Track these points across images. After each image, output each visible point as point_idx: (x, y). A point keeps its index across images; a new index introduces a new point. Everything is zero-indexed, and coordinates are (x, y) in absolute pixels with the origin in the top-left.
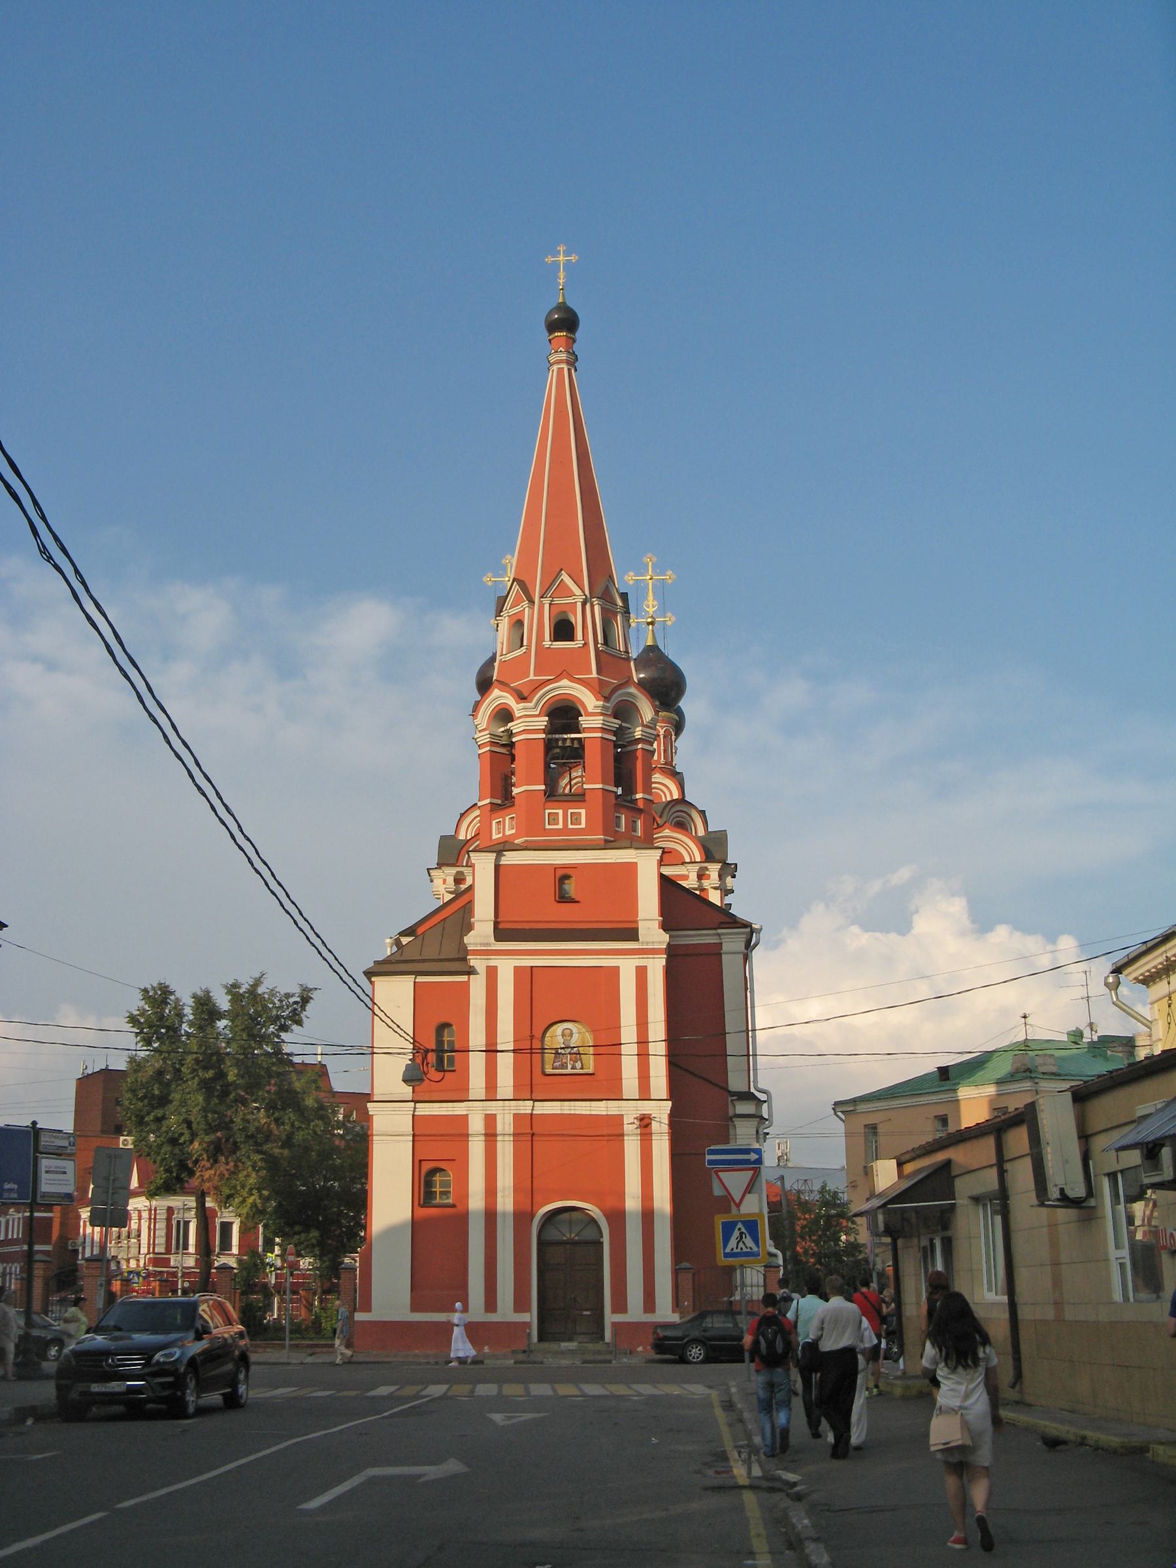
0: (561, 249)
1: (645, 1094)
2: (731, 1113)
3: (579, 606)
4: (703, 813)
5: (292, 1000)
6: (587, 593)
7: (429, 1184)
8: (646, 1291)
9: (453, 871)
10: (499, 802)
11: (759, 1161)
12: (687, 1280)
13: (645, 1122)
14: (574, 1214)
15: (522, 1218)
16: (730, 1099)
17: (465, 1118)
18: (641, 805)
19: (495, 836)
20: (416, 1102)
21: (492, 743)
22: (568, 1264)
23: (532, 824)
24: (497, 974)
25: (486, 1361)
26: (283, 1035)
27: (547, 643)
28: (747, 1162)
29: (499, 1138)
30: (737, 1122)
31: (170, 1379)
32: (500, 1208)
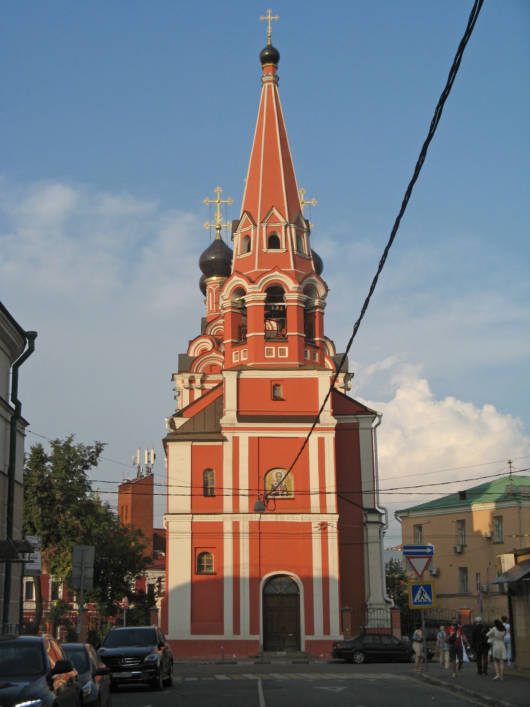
0: (269, 11)
1: (323, 510)
2: (364, 520)
3: (283, 228)
4: (332, 342)
5: (91, 450)
6: (287, 220)
7: (200, 561)
8: (324, 623)
9: (188, 375)
10: (236, 341)
11: (432, 553)
12: (348, 616)
13: (324, 526)
14: (283, 579)
15: (254, 581)
16: (364, 512)
17: (221, 523)
18: (318, 344)
19: (234, 361)
20: (193, 514)
21: (232, 307)
22: (279, 606)
23: (257, 355)
24: (239, 440)
25: (238, 663)
26: (86, 471)
27: (265, 250)
28: (426, 553)
29: (241, 535)
30: (369, 526)
31: (153, 670)
32: (241, 575)
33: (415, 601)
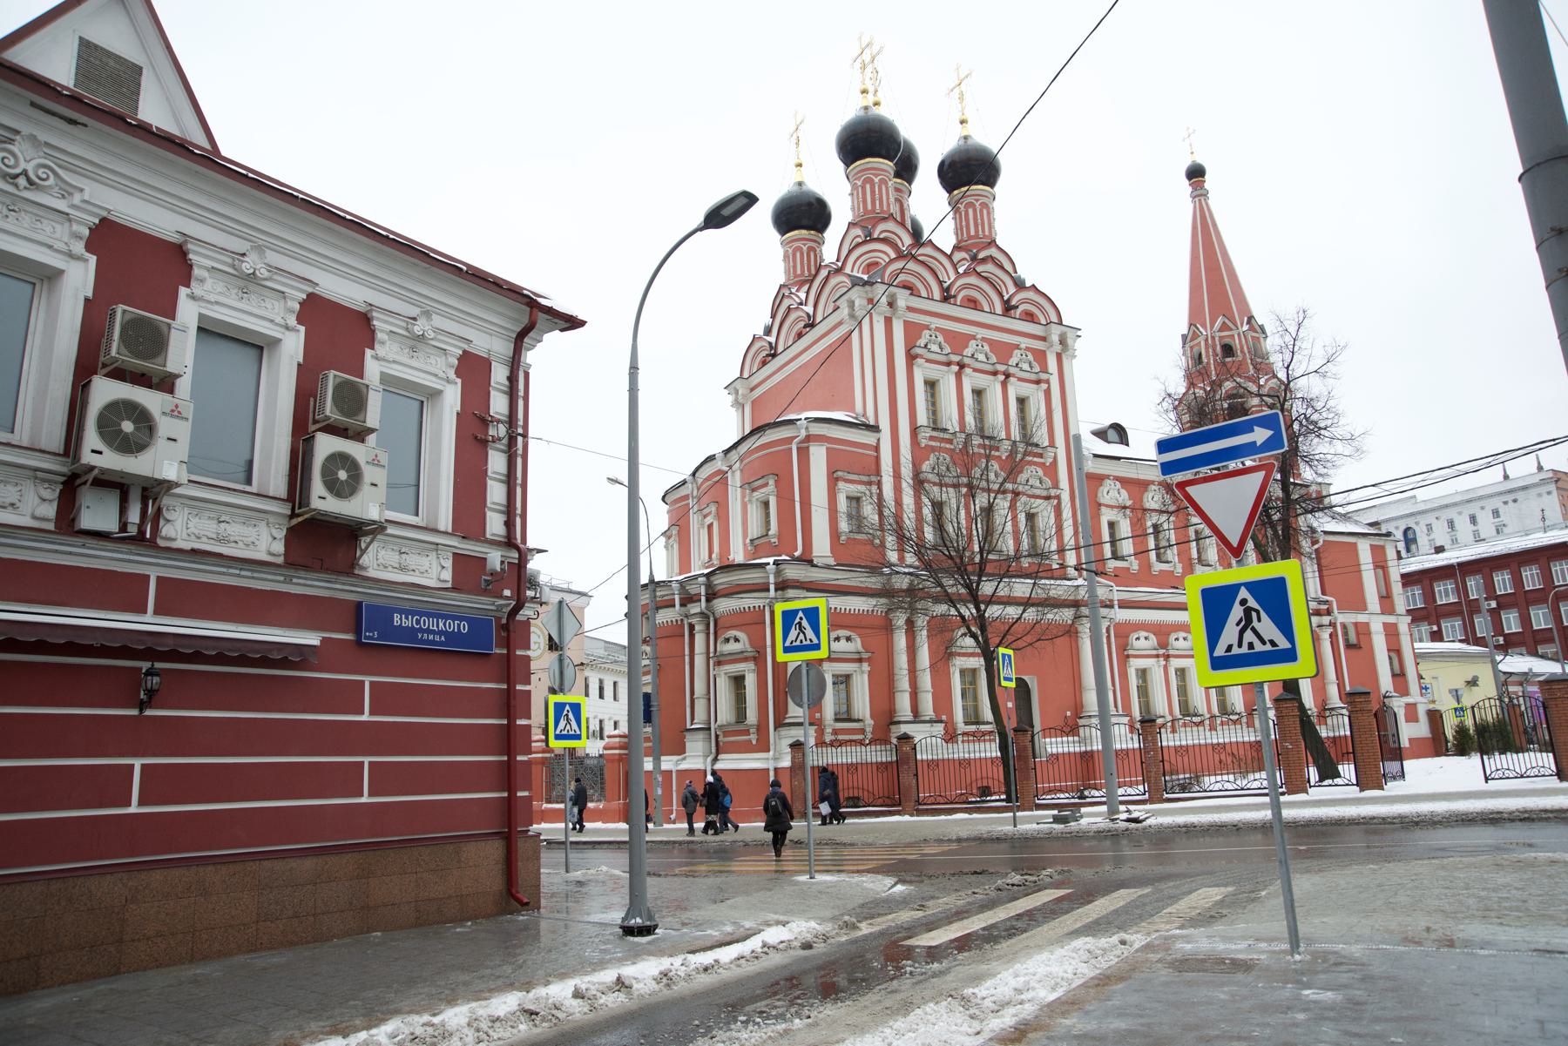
33: (1220, 651)
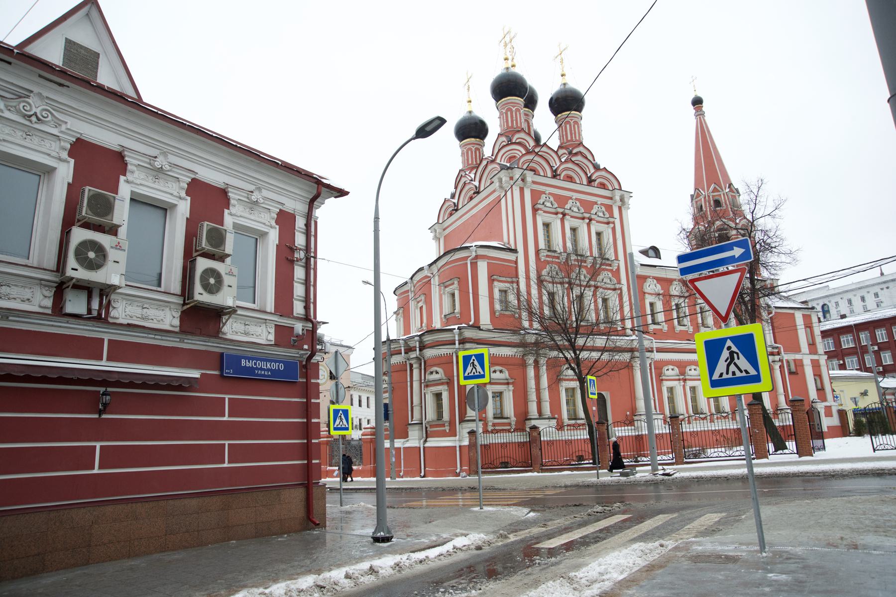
33: (716, 377)
